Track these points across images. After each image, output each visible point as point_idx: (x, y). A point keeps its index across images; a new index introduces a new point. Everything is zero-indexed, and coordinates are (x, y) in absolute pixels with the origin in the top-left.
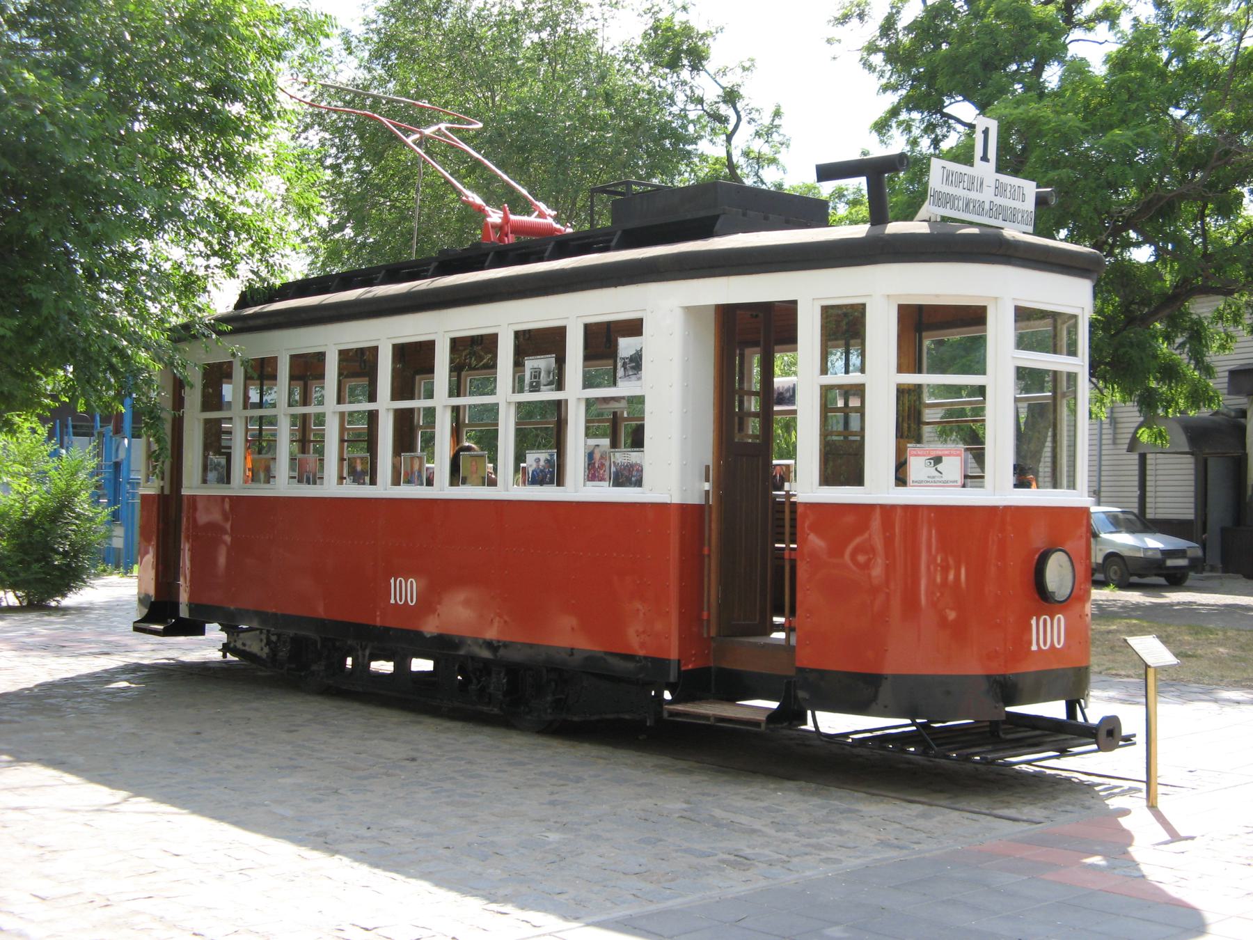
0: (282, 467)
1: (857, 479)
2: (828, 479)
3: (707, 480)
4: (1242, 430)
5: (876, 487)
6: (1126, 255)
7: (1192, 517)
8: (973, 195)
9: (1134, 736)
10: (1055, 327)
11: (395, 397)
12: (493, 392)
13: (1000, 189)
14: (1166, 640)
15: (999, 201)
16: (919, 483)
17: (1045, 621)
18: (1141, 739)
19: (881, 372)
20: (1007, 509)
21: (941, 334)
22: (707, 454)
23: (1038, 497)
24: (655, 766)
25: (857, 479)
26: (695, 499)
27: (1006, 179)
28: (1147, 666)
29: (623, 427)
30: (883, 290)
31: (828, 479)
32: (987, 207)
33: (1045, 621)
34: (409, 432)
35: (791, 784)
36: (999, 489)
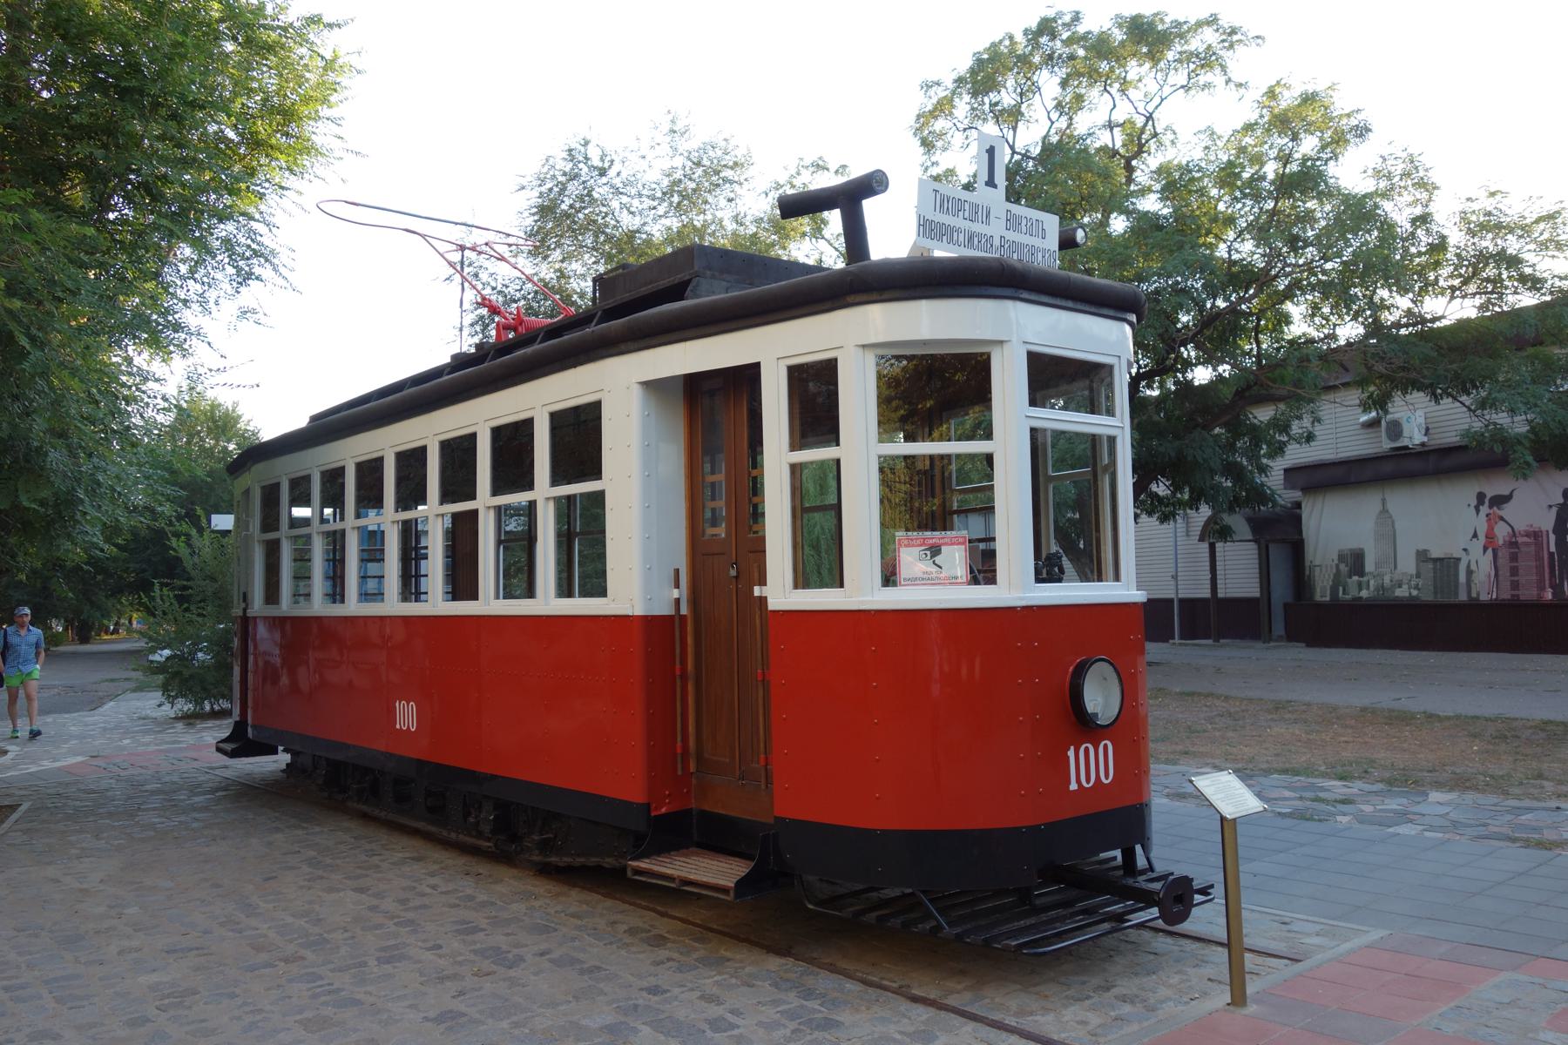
0: (319, 584)
1: (836, 579)
2: (803, 580)
3: (677, 586)
4: (1298, 519)
5: (862, 590)
6: (1189, 376)
7: (1258, 595)
8: (977, 227)
9: (1212, 886)
10: (1091, 390)
11: (474, 514)
12: (473, 497)
13: (1012, 222)
14: (1244, 775)
15: (1011, 236)
16: (913, 581)
17: (1087, 750)
18: (1218, 891)
19: (863, 446)
20: (1028, 609)
21: (939, 390)
22: (680, 558)
23: (1072, 592)
24: (632, 931)
25: (836, 579)
26: (663, 608)
27: (1020, 210)
28: (1223, 819)
29: (584, 529)
30: (854, 340)
31: (803, 580)
32: (997, 242)
33: (1087, 750)
34: (518, 547)
35: (774, 963)
36: (1016, 586)
